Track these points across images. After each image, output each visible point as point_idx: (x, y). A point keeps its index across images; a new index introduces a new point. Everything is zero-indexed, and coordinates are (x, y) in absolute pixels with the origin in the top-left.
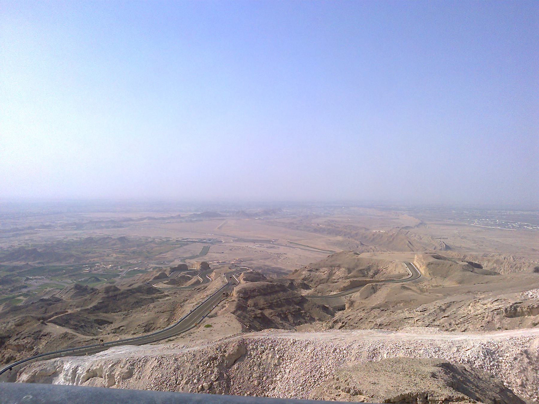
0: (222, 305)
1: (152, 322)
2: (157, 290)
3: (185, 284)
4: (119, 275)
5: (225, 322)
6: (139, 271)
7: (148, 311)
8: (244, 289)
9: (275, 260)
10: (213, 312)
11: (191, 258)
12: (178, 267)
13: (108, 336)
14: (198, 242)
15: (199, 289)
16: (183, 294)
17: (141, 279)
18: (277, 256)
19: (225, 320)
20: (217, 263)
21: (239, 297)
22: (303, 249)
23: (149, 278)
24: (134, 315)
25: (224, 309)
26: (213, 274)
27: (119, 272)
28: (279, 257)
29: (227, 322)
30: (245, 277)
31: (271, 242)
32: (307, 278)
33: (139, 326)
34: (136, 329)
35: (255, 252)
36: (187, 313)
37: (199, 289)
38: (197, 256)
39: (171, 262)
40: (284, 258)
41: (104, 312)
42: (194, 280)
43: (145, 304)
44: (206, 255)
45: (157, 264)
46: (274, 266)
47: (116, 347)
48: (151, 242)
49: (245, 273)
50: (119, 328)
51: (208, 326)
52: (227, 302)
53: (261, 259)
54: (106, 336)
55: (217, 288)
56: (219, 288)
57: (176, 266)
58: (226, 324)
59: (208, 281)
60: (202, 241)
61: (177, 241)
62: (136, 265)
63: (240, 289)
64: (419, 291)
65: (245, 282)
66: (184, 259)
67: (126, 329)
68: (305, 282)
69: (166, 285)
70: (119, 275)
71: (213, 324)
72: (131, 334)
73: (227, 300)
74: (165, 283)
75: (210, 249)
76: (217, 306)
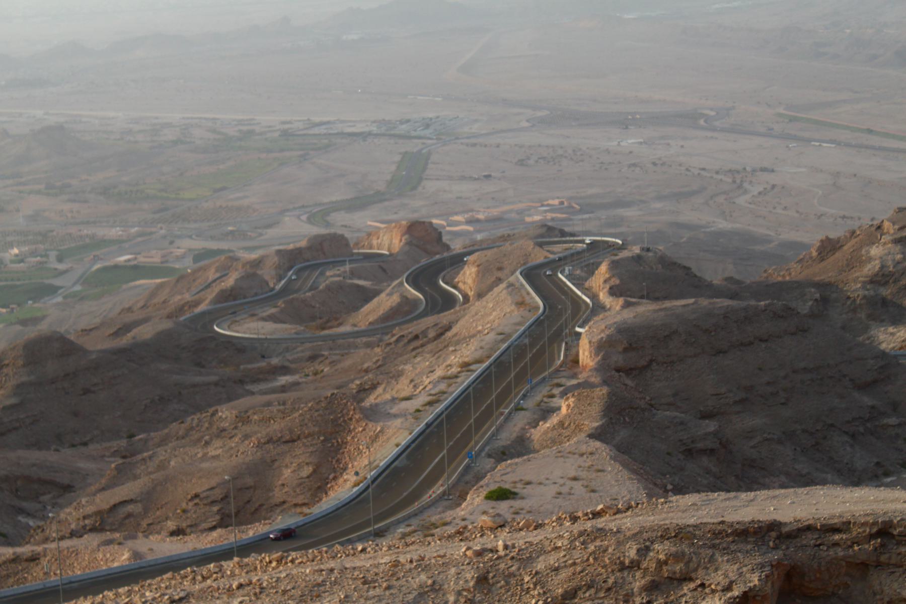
0: (539, 405)
1: (249, 481)
2: (237, 347)
3: (351, 321)
4: (53, 290)
5: (573, 474)
6: (135, 267)
7: (218, 436)
8: (624, 330)
9: (721, 199)
10: (506, 437)
11: (354, 205)
12: (309, 248)
13: (74, 542)
14: (377, 135)
15: (416, 337)
16: (348, 363)
17: (155, 301)
18: (730, 180)
19: (570, 467)
20: (469, 222)
21: (601, 368)
22: (848, 145)
23: (188, 297)
24: (162, 454)
25: (554, 420)
26: (468, 277)
27: (56, 276)
28: (740, 187)
29: (583, 474)
30: (616, 281)
31: (702, 122)
32: (892, 274)
33: (197, 501)
34: (184, 511)
35: (630, 166)
36: (394, 441)
37: (416, 337)
38: (378, 198)
39: (269, 226)
40: (761, 189)
41: (29, 446)
42: (384, 302)
43: (199, 409)
44: (414, 188)
45: (213, 238)
46: (723, 225)
47: (9, 594)
48: (175, 143)
49: (614, 265)
50: (115, 507)
51: (501, 495)
52: (556, 391)
53: (660, 198)
54: (65, 544)
55: (500, 330)
56: (507, 330)
57: (303, 244)
58: (577, 485)
59: (448, 302)
60: (396, 132)
61: (285, 134)
62: (118, 244)
63: (607, 332)
64: (690, 168)
65: (621, 301)
66: (320, 214)
67: (146, 510)
68: (886, 292)
69: (270, 326)
70: (53, 290)
71: (519, 485)
72: (164, 533)
73: (556, 381)
74: (264, 319)
75: (430, 166)
76: (518, 409)
